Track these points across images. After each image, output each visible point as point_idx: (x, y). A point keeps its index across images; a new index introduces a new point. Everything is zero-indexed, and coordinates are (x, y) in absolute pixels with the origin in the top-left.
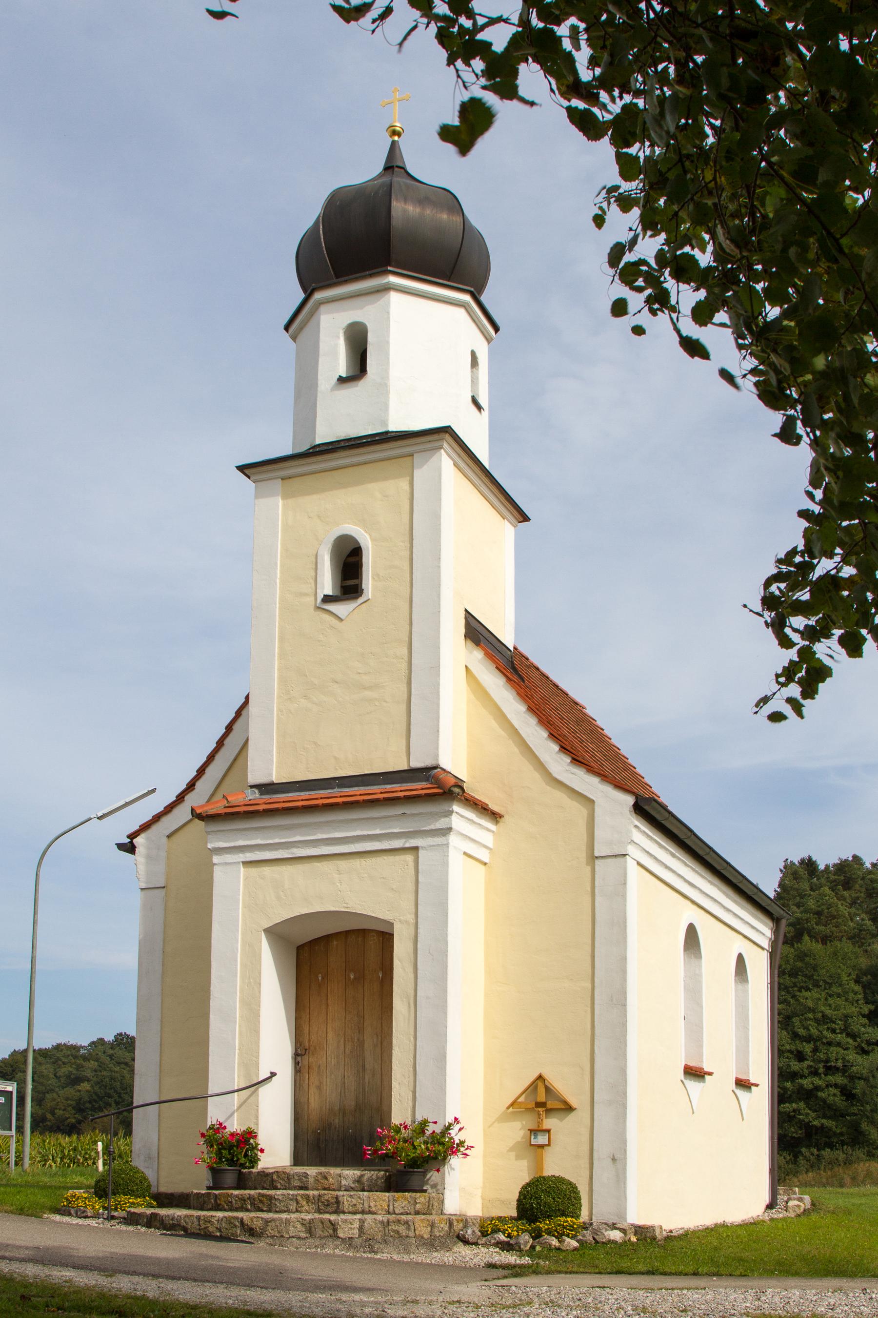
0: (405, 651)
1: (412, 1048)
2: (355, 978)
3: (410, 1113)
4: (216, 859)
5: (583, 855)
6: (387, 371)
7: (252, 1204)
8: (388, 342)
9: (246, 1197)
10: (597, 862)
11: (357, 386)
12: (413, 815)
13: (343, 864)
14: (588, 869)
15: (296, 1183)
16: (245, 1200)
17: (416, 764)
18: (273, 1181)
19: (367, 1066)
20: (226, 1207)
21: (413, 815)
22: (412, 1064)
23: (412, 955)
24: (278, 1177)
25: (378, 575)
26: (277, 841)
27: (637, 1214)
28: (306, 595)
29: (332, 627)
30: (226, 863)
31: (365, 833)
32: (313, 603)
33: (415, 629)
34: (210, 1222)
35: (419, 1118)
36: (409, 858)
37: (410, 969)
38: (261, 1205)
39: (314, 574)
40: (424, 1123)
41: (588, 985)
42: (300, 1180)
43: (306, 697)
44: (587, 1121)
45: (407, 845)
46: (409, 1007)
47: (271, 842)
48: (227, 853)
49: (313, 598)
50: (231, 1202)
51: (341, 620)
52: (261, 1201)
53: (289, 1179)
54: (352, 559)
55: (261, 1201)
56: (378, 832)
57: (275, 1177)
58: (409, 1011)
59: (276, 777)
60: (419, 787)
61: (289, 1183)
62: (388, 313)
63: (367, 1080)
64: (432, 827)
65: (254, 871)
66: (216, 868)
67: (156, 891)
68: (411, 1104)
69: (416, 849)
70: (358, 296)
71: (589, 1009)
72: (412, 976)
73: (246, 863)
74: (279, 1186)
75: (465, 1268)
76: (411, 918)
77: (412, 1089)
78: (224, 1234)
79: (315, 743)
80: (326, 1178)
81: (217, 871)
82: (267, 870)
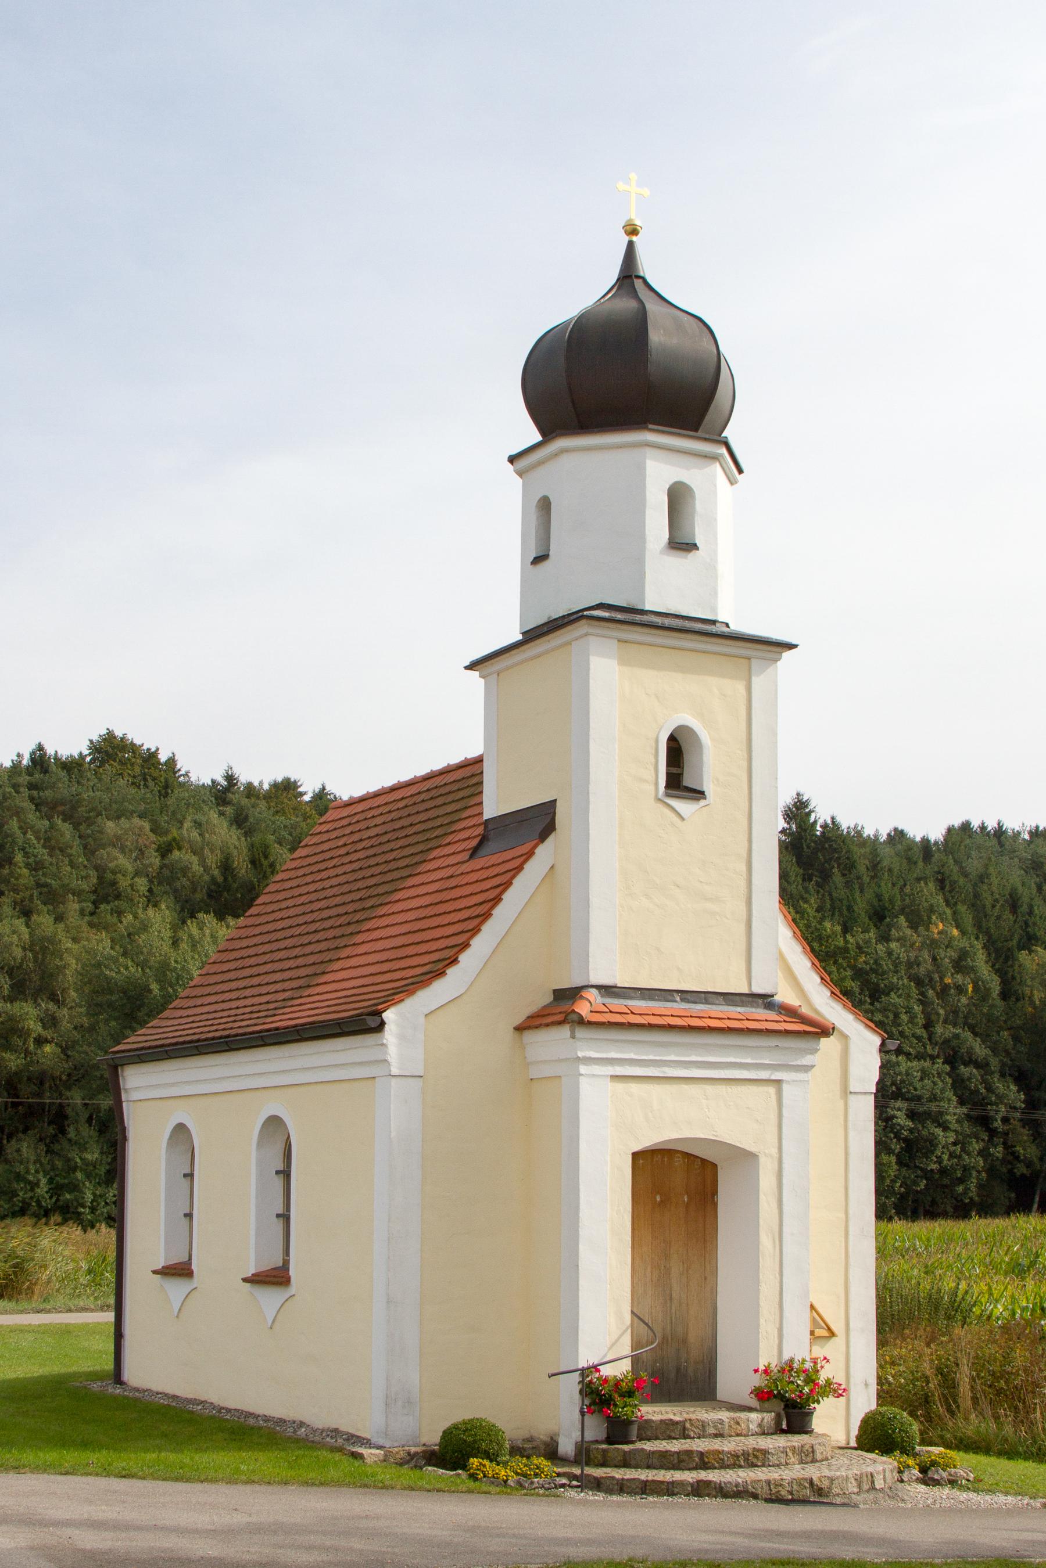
0: (743, 868)
1: (778, 1285)
2: (661, 1201)
3: (775, 1352)
4: (583, 1069)
5: (837, 1088)
6: (715, 552)
7: (746, 1460)
8: (716, 520)
9: (740, 1454)
10: (851, 1098)
11: (686, 558)
12: (786, 1048)
13: (709, 1089)
14: (841, 1103)
15: (712, 1431)
16: (738, 1457)
17: (756, 989)
18: (684, 1428)
19: (674, 1295)
20: (717, 1465)
21: (786, 1048)
22: (777, 1299)
23: (776, 1190)
24: (692, 1425)
25: (718, 780)
26: (651, 1057)
27: (112, 1367)
28: (646, 781)
29: (673, 825)
30: (594, 1075)
31: (738, 1060)
32: (653, 793)
33: (754, 847)
34: (781, 1485)
35: (786, 1357)
36: (772, 1090)
37: (774, 1205)
38: (755, 1461)
39: (653, 760)
40: (792, 1360)
41: (843, 1216)
42: (715, 1427)
43: (647, 896)
44: (843, 1348)
45: (773, 1077)
46: (774, 1242)
47: (646, 1058)
48: (595, 1064)
49: (652, 788)
50: (723, 1460)
51: (683, 819)
52: (756, 1457)
53: (703, 1426)
54: (675, 745)
55: (756, 1457)
56: (749, 1061)
57: (688, 1425)
58: (775, 1247)
59: (622, 980)
60: (688, 996)
61: (704, 1431)
62: (715, 486)
63: (673, 1311)
64: (799, 1063)
65: (620, 1086)
66: (582, 1080)
67: (410, 1080)
68: (777, 1341)
69: (779, 1082)
70: (685, 453)
71: (843, 1240)
72: (776, 1211)
73: (615, 1078)
74: (692, 1434)
75: (976, 1511)
76: (774, 1151)
77: (778, 1326)
78: (795, 1497)
79: (658, 949)
80: (738, 1423)
81: (583, 1081)
82: (634, 1087)
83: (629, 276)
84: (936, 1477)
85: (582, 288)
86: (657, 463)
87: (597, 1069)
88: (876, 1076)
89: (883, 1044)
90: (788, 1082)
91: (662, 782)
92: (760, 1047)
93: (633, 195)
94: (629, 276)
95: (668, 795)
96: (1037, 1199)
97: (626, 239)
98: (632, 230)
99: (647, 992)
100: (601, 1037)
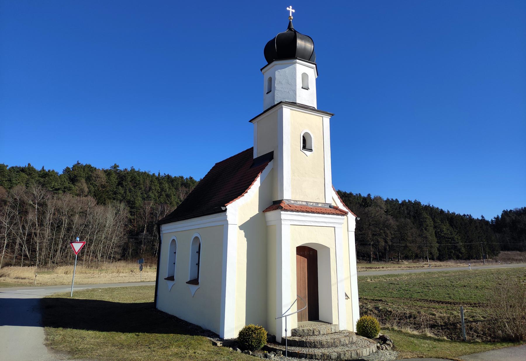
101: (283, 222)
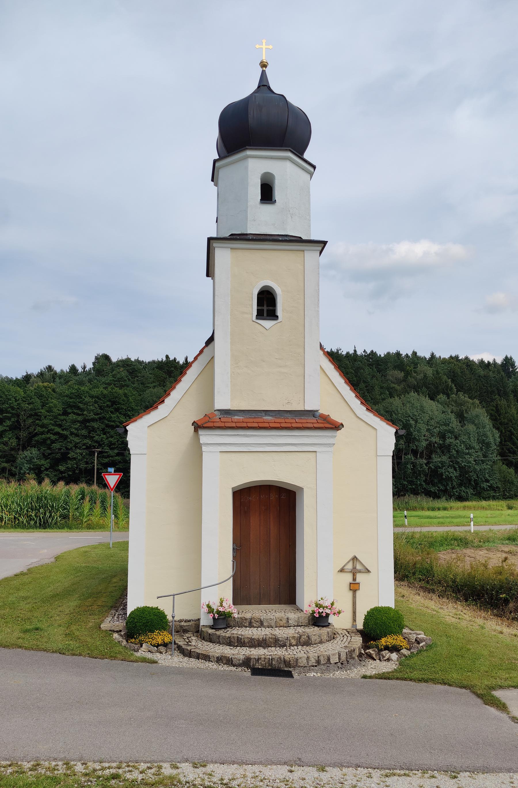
17: (307, 408)
57: (253, 621)
83: (264, 84)
84: (90, 600)
85: (245, 88)
86: (279, 166)
87: (211, 448)
88: (393, 448)
89: (396, 433)
90: (320, 452)
91: (255, 313)
92: (328, 436)
93: (264, 50)
94: (264, 84)
95: (257, 318)
96: (95, 480)
97: (261, 70)
98: (264, 65)
99: (277, 412)
100: (316, 434)
101: (204, 448)
